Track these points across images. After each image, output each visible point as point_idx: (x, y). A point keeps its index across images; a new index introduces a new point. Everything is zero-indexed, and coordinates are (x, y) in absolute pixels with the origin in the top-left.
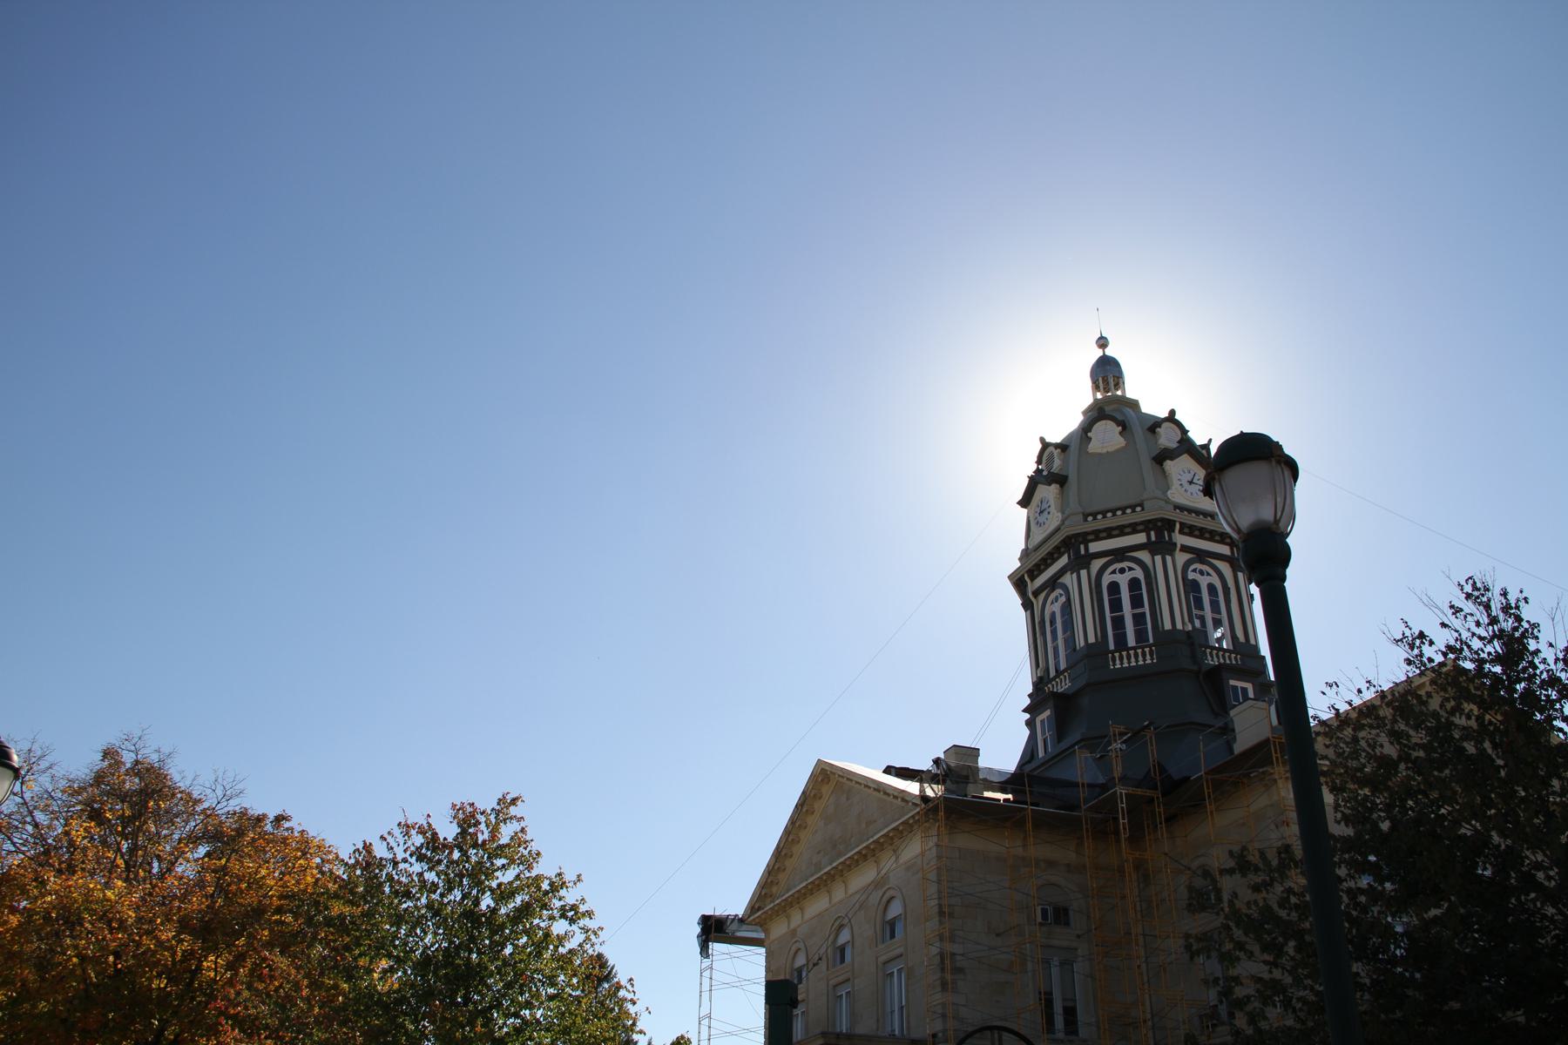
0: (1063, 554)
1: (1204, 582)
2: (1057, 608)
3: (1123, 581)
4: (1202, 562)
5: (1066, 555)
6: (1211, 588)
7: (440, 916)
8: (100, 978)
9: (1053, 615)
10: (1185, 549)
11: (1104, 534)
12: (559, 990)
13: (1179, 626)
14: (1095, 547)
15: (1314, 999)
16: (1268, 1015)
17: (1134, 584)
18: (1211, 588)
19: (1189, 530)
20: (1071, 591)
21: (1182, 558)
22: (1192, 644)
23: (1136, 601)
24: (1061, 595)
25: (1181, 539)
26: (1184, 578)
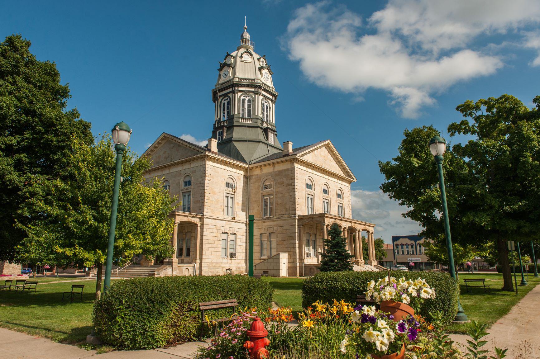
0: (231, 88)
1: (266, 104)
2: (226, 102)
3: (247, 99)
4: (266, 99)
5: (232, 88)
6: (267, 106)
7: (441, 160)
8: (473, 263)
9: (224, 104)
10: (263, 95)
11: (250, 86)
12: (271, 290)
13: (259, 115)
14: (240, 89)
15: (464, 260)
16: (400, 280)
17: (249, 101)
18: (267, 106)
19: (265, 90)
20: (232, 99)
21: (262, 97)
22: (262, 121)
23: (249, 106)
24: (228, 99)
25: (263, 92)
26: (261, 103)
